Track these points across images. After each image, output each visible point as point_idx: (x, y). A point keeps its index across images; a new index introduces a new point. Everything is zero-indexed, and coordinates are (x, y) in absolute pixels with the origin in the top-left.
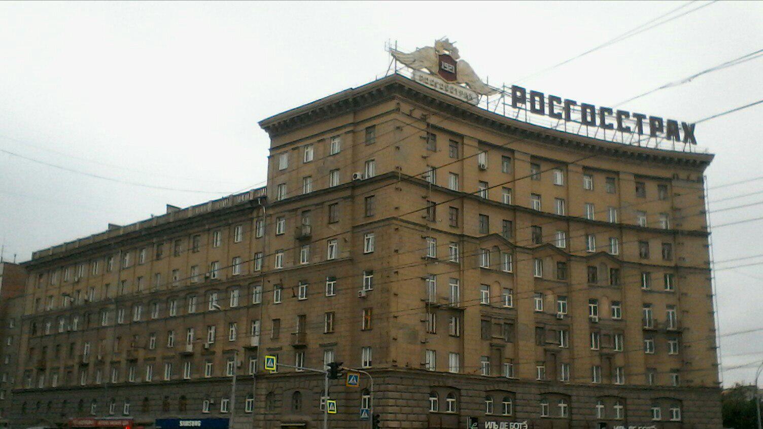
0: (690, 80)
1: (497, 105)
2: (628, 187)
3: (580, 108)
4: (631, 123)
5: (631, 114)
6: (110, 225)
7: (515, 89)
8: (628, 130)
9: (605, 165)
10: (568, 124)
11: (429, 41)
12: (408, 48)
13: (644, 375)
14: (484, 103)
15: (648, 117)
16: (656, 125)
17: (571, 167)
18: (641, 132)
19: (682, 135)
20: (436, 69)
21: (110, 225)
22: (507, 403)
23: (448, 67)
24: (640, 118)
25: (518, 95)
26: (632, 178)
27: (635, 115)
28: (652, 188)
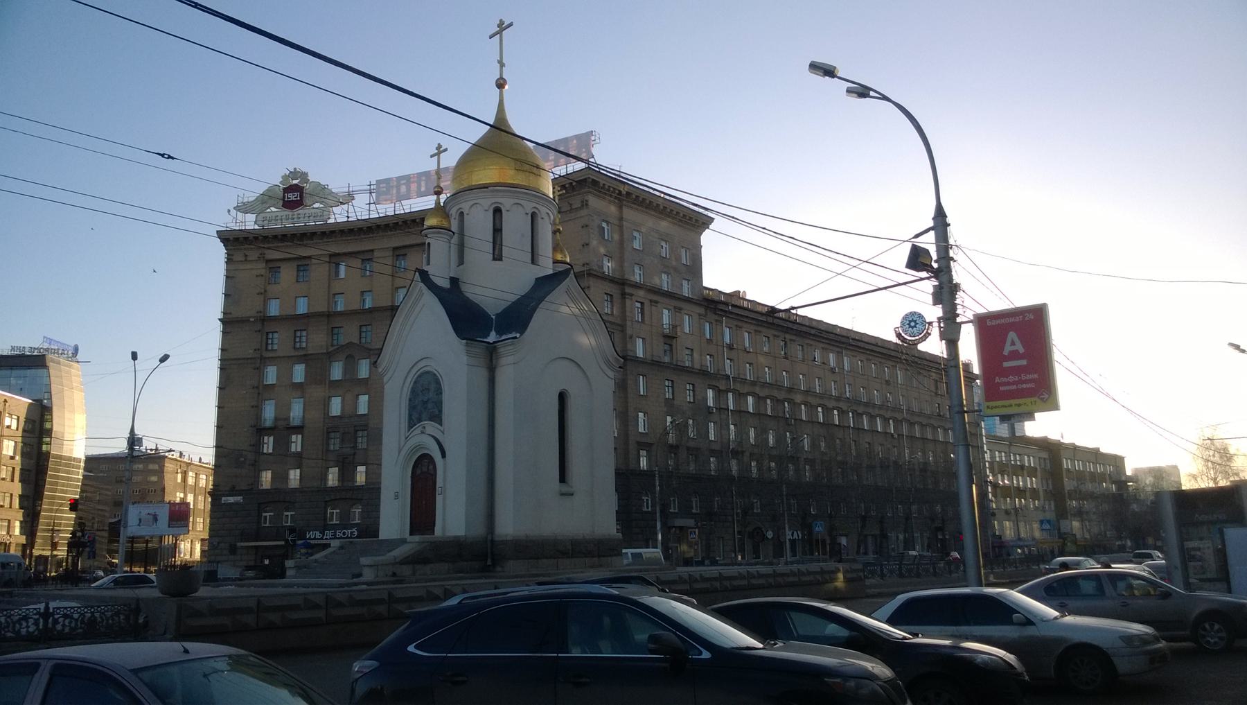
1: (361, 210)
11: (274, 177)
14: (339, 215)
20: (281, 203)
23: (292, 197)
25: (382, 189)
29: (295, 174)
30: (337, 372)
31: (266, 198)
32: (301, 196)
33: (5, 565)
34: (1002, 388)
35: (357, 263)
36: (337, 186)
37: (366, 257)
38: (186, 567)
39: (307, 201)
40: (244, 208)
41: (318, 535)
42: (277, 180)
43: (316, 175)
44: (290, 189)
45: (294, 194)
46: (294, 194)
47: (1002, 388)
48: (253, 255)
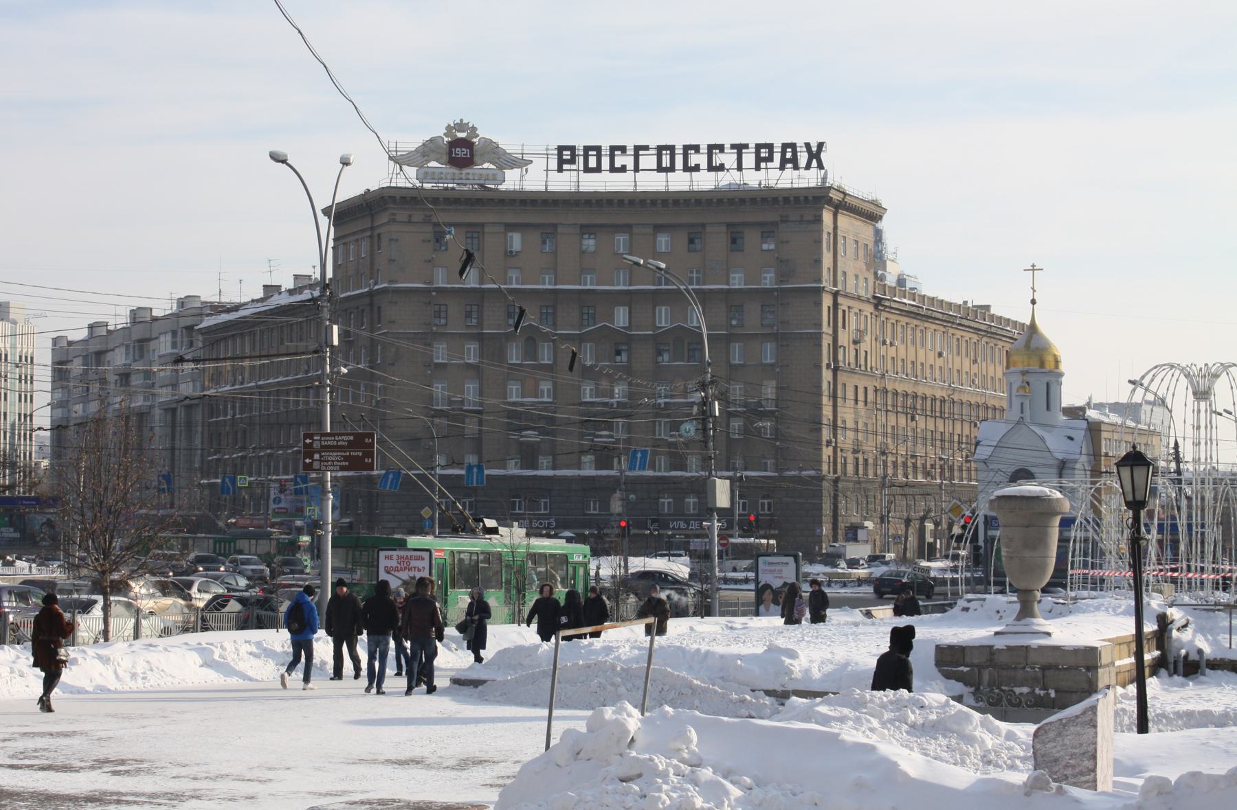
0: (41, 802)
1: (538, 177)
2: (717, 240)
3: (655, 152)
4: (729, 159)
5: (727, 146)
6: (296, 277)
7: (561, 149)
8: (721, 168)
9: (685, 219)
10: (640, 175)
11: (437, 130)
12: (411, 142)
13: (728, 482)
14: (512, 181)
15: (752, 145)
16: (763, 154)
17: (635, 230)
18: (740, 168)
19: (803, 158)
20: (445, 158)
21: (296, 277)
22: (583, 473)
23: (460, 152)
24: (740, 148)
25: (565, 156)
26: (724, 229)
27: (733, 146)
28: (751, 238)
29: (461, 126)
30: (514, 355)
31: (428, 149)
32: (450, 153)
33: (1236, 684)
34: (329, 275)
35: (535, 237)
36: (509, 144)
37: (549, 231)
38: (57, 654)
39: (476, 159)
40: (399, 160)
41: (683, 525)
42: (440, 131)
43: (485, 132)
44: (456, 143)
45: (461, 149)
46: (461, 149)
47: (329, 275)
48: (418, 216)
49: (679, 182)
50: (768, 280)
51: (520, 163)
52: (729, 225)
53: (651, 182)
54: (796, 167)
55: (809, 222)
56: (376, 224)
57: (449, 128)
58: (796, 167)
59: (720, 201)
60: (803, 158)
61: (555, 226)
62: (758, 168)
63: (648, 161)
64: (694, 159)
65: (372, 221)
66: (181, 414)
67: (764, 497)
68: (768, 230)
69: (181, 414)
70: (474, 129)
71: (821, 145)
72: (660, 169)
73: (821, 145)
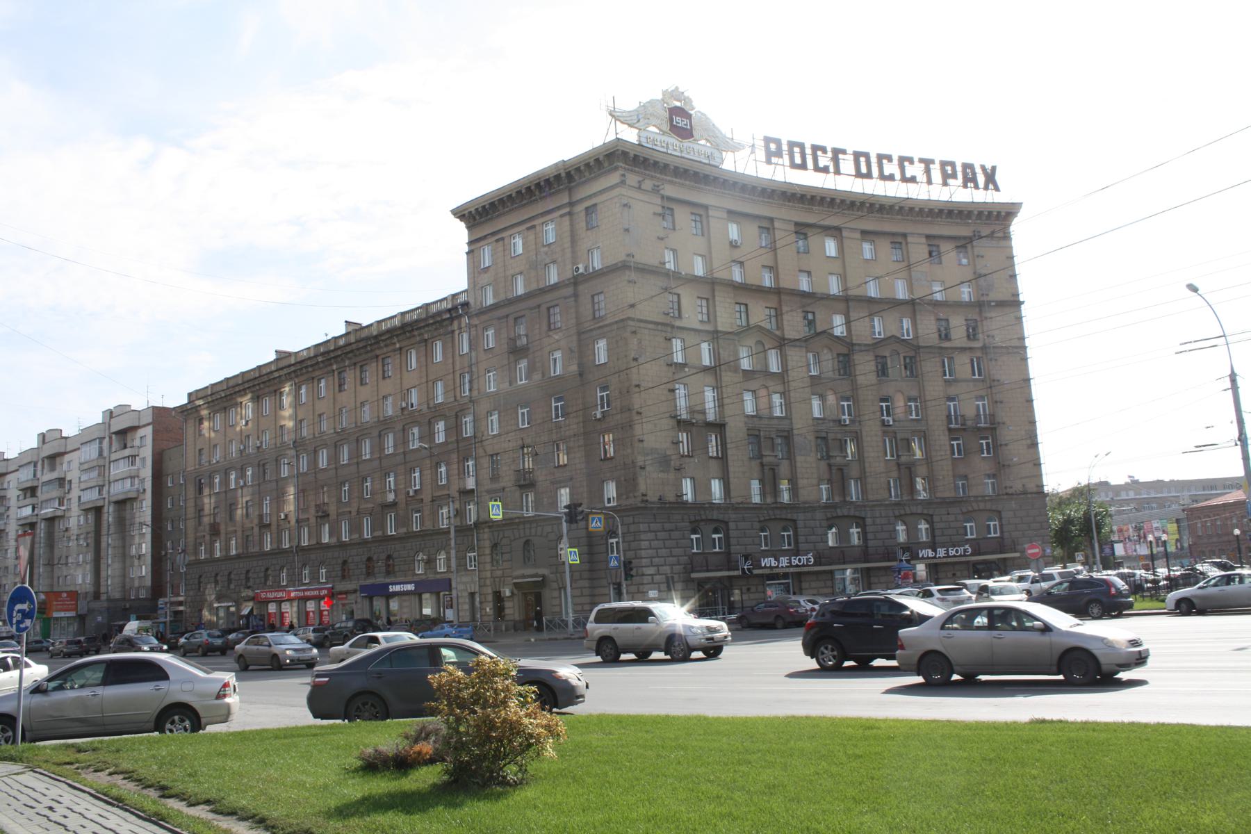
2: (918, 250)
4: (915, 170)
5: (916, 160)
7: (768, 140)
11: (653, 92)
12: (628, 104)
19: (981, 180)
20: (666, 127)
25: (773, 148)
35: (885, 245)
37: (899, 240)
40: (631, 120)
44: (675, 112)
46: (679, 119)
49: (873, 187)
50: (965, 293)
51: (735, 148)
52: (928, 237)
53: (846, 183)
54: (976, 187)
55: (1000, 238)
56: (574, 199)
57: (665, 93)
58: (976, 187)
59: (950, 213)
60: (981, 180)
61: (904, 235)
62: (945, 184)
63: (847, 164)
64: (889, 168)
65: (570, 196)
66: (109, 515)
67: (558, 400)
68: (963, 244)
69: (109, 515)
70: (691, 101)
71: (994, 168)
72: (859, 174)
73: (994, 168)
